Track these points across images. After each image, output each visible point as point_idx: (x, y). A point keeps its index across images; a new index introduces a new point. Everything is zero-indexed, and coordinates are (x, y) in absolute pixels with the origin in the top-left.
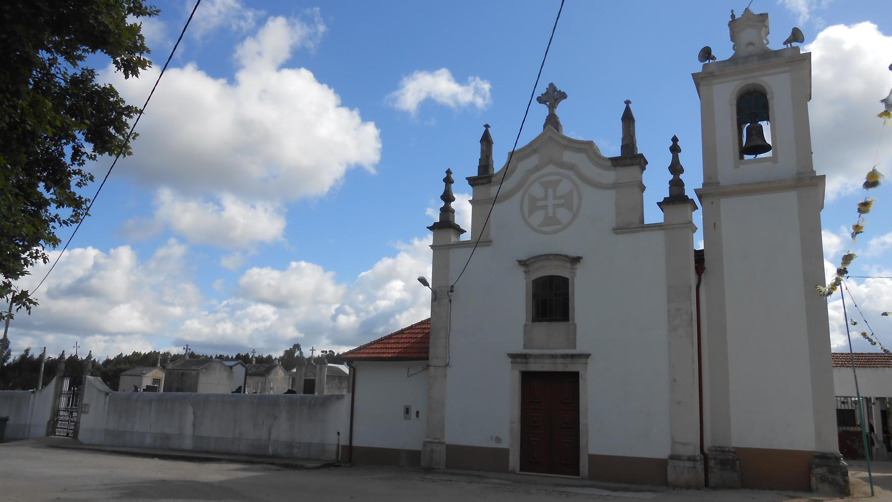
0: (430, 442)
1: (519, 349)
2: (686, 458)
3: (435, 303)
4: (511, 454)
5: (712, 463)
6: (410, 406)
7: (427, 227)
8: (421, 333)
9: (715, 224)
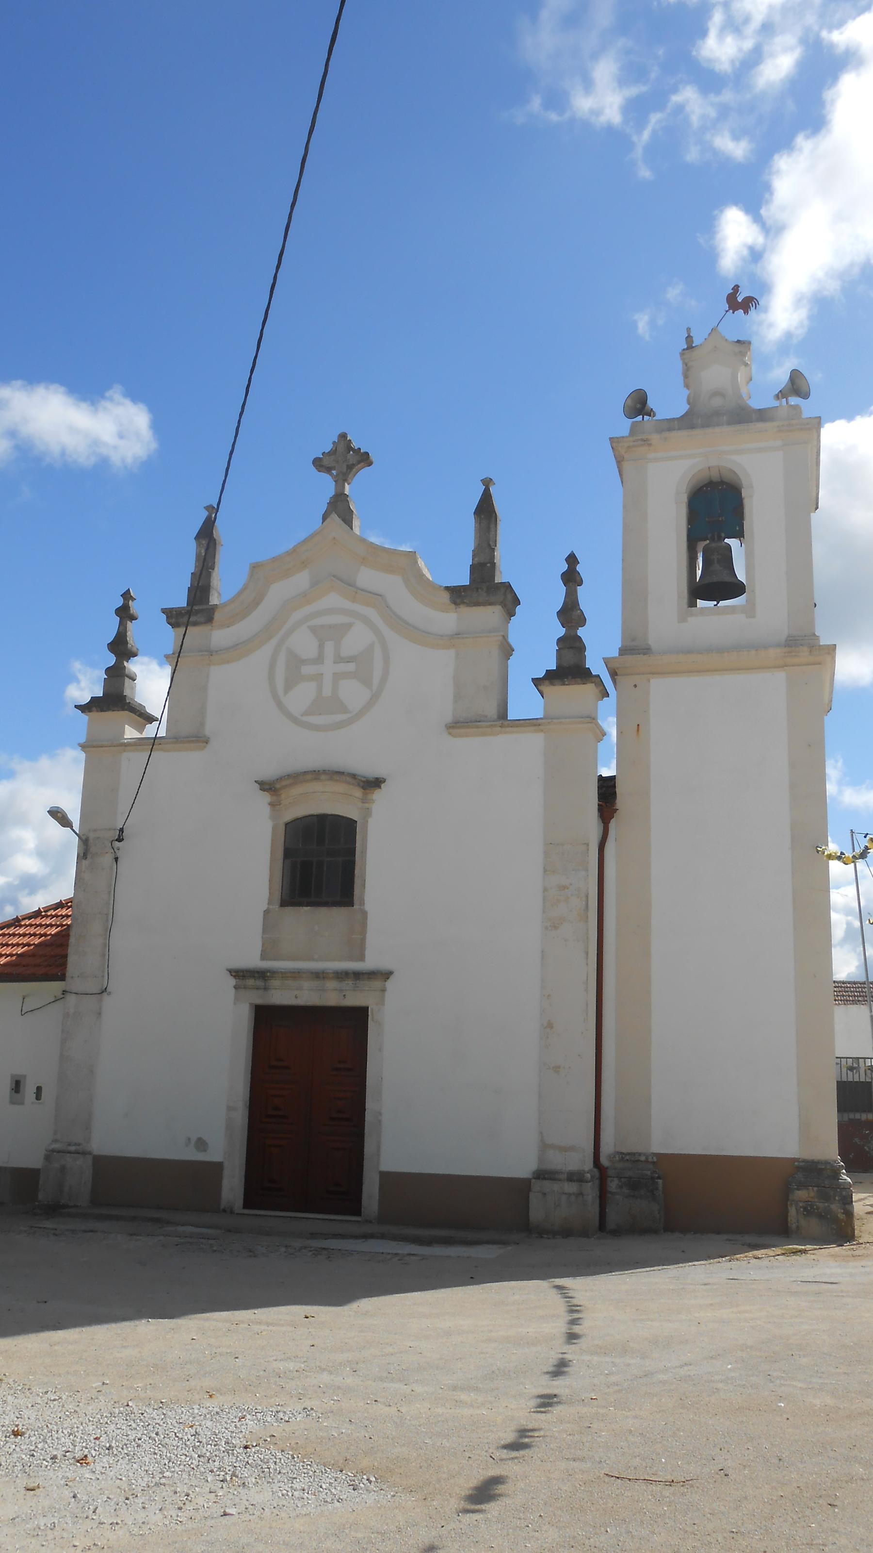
0: (59, 1152)
1: (252, 959)
2: (565, 1176)
3: (85, 863)
4: (226, 1173)
5: (613, 1185)
6: (24, 1077)
7: (76, 706)
8: (58, 926)
9: (638, 725)
